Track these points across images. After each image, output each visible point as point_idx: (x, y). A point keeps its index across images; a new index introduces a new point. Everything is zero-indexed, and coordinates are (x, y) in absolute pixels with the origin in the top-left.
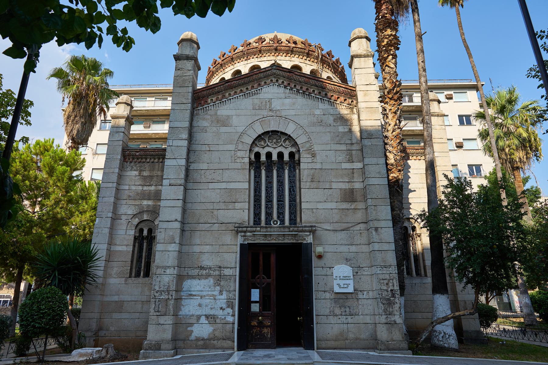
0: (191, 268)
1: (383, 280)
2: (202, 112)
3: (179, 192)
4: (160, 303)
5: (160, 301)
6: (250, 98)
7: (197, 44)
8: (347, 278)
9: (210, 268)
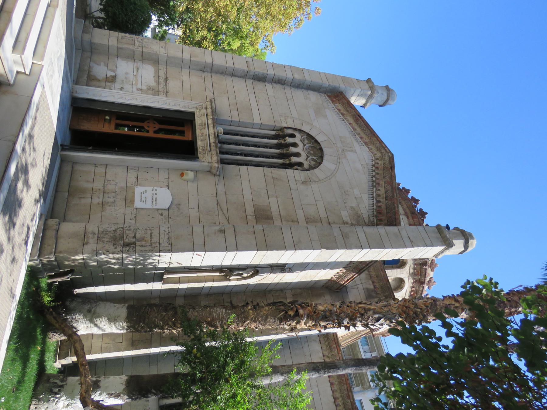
1: (151, 233)
8: (154, 201)
9: (166, 85)
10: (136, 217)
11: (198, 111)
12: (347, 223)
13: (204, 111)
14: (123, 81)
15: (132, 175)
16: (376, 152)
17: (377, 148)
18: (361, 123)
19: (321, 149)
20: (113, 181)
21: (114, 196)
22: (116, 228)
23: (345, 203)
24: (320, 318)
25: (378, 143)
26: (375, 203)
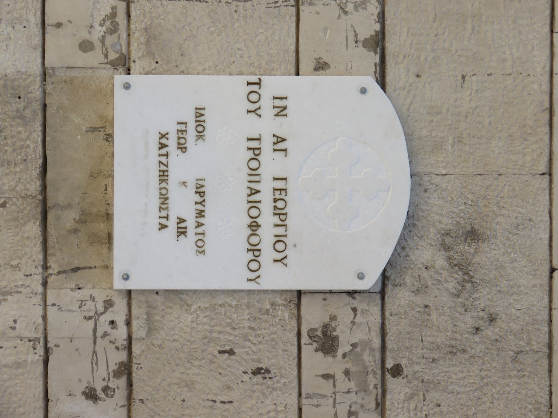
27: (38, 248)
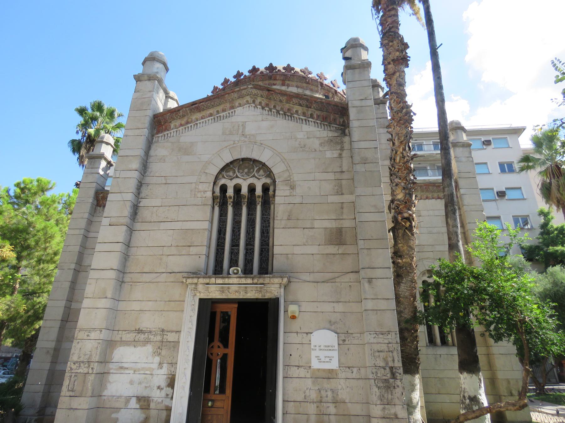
0: (126, 332)
1: (378, 352)
2: (162, 139)
3: (120, 233)
4: (76, 378)
5: (76, 376)
6: (220, 121)
7: (165, 64)
8: (329, 348)
9: (150, 332)
10: (349, 368)
11: (198, 294)
12: (340, 154)
13: (200, 287)
14: (146, 387)
15: (294, 372)
16: (245, 101)
17: (239, 98)
18: (203, 105)
19: (243, 160)
20: (305, 392)
21: (324, 391)
22: (375, 387)
23: (315, 151)
24: (410, 199)
25: (232, 94)
26: (314, 121)
27: (333, 379)
